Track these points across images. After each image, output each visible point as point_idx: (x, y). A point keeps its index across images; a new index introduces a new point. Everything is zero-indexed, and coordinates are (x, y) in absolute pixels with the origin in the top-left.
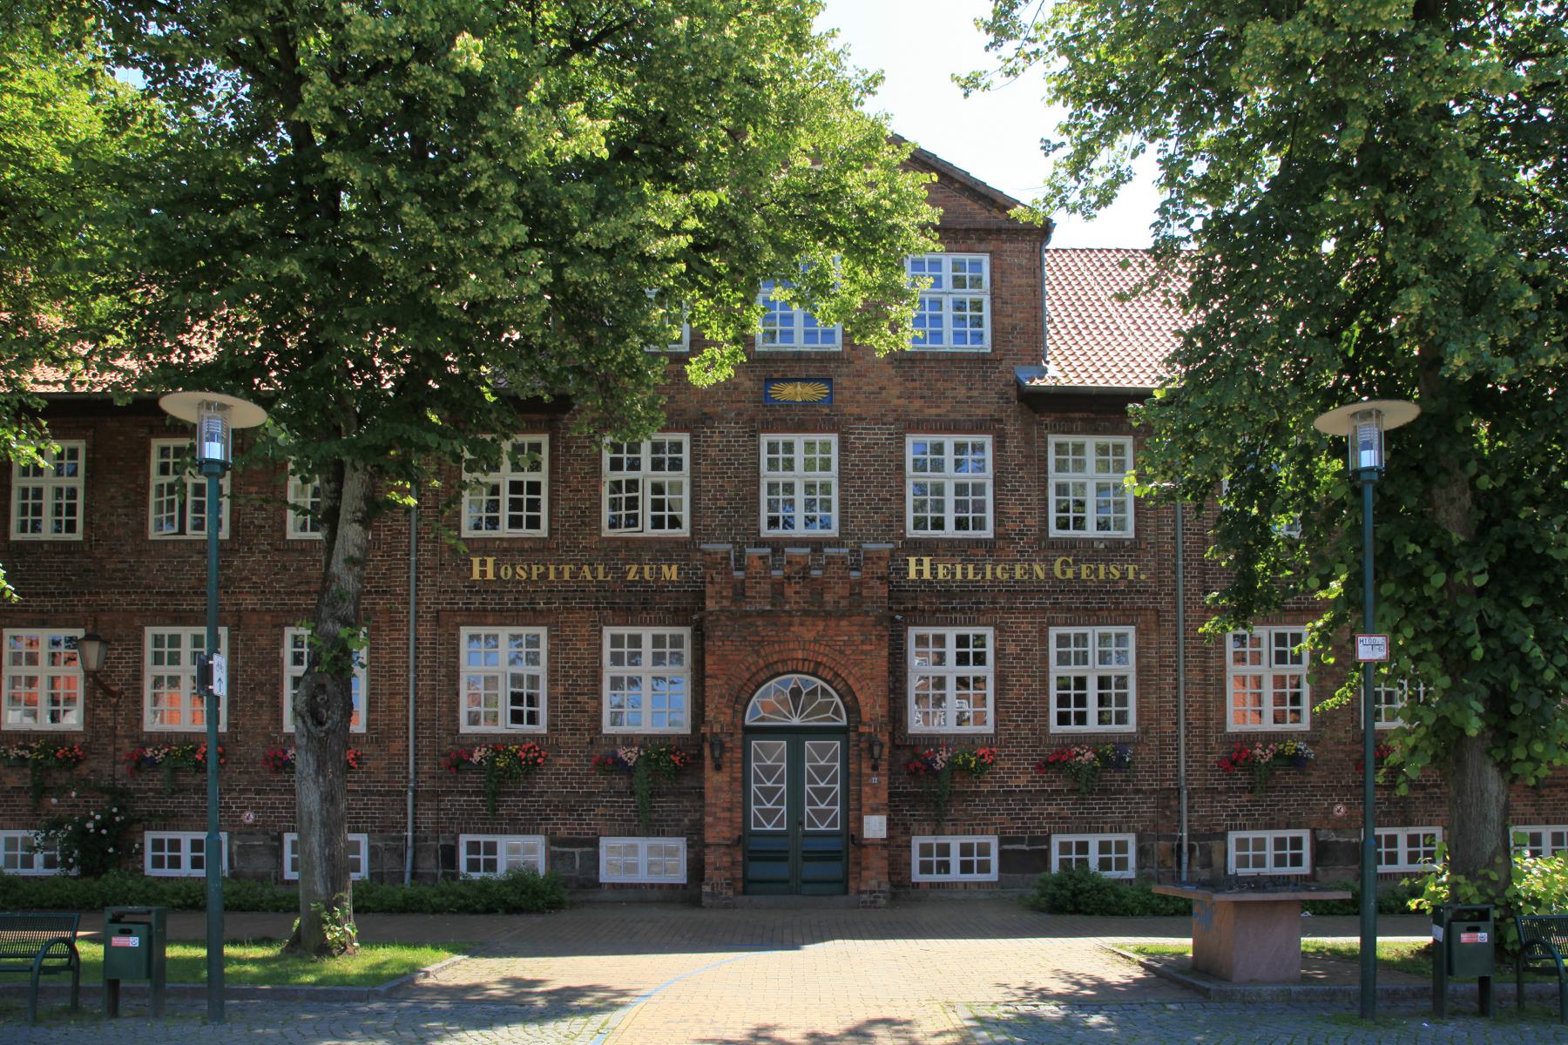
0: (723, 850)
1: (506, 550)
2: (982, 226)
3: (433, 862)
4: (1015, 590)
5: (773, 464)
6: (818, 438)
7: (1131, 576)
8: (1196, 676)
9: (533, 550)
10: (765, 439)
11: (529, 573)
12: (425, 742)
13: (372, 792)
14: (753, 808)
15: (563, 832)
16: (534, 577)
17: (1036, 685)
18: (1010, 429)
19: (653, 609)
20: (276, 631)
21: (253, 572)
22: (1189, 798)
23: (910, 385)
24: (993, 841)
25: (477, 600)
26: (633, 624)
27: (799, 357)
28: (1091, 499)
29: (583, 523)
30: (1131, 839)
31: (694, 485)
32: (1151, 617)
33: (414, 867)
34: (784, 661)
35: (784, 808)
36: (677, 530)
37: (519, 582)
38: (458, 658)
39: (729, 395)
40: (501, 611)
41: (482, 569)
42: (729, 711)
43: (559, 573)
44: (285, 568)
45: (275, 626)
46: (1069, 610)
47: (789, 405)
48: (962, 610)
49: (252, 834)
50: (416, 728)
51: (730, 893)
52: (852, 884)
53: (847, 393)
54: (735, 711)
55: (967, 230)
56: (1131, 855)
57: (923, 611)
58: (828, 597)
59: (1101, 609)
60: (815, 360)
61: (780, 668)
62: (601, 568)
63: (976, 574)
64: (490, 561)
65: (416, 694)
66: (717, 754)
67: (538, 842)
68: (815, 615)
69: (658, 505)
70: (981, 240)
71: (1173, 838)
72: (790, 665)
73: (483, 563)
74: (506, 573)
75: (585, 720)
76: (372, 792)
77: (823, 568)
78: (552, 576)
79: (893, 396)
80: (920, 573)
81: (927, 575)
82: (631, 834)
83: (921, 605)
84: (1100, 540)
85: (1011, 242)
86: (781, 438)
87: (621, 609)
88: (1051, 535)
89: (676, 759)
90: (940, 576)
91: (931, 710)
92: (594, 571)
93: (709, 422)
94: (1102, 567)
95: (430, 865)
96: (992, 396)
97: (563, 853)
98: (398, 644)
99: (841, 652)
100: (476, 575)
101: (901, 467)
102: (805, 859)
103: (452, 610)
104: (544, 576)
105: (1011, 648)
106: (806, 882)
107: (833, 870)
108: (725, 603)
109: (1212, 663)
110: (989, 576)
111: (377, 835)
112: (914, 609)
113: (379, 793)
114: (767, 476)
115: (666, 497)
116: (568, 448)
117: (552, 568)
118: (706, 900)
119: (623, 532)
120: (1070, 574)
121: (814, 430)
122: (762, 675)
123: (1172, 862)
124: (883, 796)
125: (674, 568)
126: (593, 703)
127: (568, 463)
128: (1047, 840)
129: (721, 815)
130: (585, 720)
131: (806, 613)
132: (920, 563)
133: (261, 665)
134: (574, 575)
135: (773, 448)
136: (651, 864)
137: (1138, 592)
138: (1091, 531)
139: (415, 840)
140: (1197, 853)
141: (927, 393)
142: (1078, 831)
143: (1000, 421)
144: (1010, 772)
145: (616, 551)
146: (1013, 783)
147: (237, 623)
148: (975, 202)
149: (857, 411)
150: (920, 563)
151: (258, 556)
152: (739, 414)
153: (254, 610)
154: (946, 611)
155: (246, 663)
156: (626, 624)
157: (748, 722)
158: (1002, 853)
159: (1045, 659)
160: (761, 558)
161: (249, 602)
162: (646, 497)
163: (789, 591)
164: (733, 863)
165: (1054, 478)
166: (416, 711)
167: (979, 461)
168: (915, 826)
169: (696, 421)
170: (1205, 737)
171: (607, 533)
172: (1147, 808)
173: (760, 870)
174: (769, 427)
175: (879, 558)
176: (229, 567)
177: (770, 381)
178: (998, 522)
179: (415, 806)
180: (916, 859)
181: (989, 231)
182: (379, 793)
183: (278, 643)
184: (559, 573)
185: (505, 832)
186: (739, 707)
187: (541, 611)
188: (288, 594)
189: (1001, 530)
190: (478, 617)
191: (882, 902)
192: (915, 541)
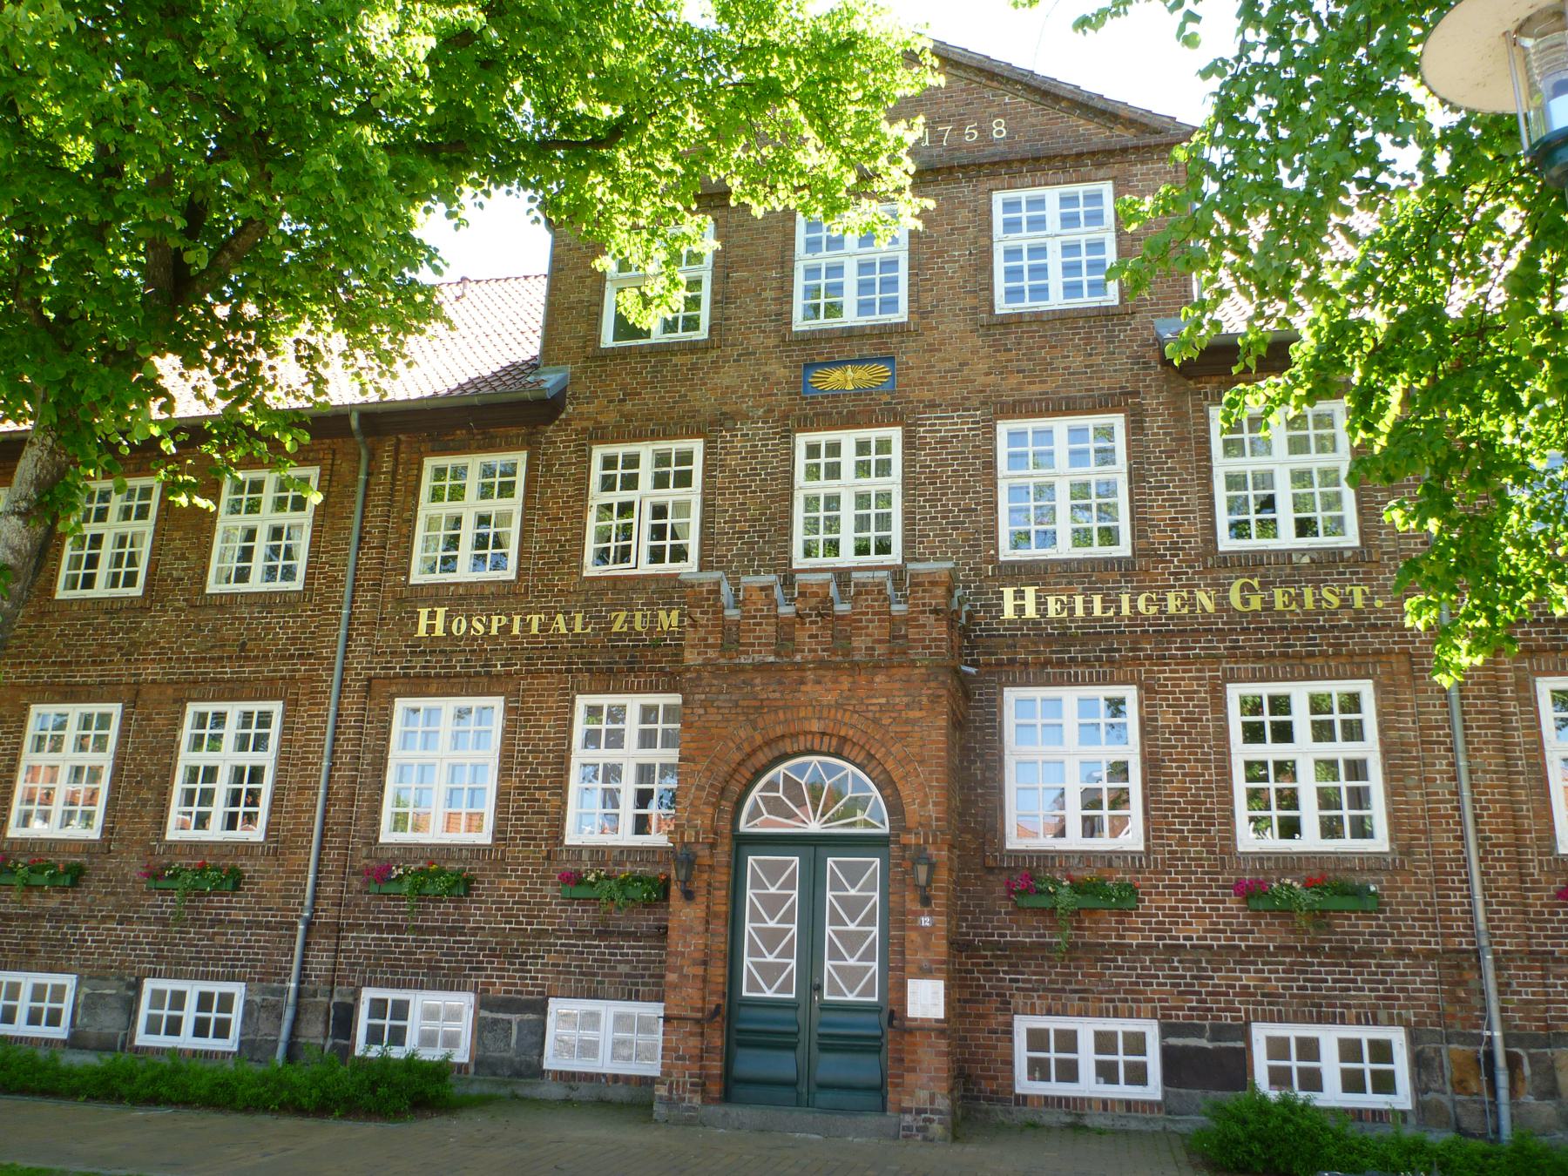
1: (462, 598)
2: (1100, 147)
3: (320, 1028)
4: (1166, 632)
5: (812, 473)
6: (872, 434)
7: (1359, 603)
8: (1489, 758)
9: (496, 596)
10: (802, 440)
11: (488, 627)
12: (333, 854)
13: (259, 925)
15: (498, 990)
16: (494, 632)
17: (1211, 774)
18: (1150, 402)
19: (642, 670)
20: (176, 707)
21: (162, 635)
22: (1499, 968)
23: (1002, 356)
24: (1151, 1030)
25: (418, 663)
26: (617, 691)
27: (850, 333)
28: (1284, 493)
29: (562, 559)
30: (1397, 1037)
31: (707, 505)
32: (1400, 665)
33: (293, 1033)
34: (794, 736)
35: (793, 962)
36: (682, 564)
37: (475, 638)
38: (387, 740)
39: (756, 388)
40: (447, 676)
41: (430, 622)
42: (709, 810)
43: (526, 625)
44: (199, 628)
45: (175, 701)
46: (1258, 657)
47: (836, 396)
48: (1085, 661)
49: (105, 979)
50: (323, 835)
51: (697, 1099)
52: (891, 1096)
53: (914, 374)
55: (1080, 155)
56: (1401, 1066)
57: (1026, 664)
58: (859, 642)
59: (1311, 655)
60: (871, 336)
61: (788, 746)
62: (579, 617)
63: (1105, 609)
64: (441, 612)
65: (328, 788)
67: (464, 1001)
68: (836, 667)
69: (658, 532)
70: (1099, 165)
71: (1478, 1039)
72: (802, 743)
73: (432, 616)
74: (459, 627)
75: (542, 825)
76: (259, 925)
77: (854, 600)
78: (516, 631)
79: (980, 372)
80: (1020, 609)
81: (1031, 612)
82: (593, 995)
84: (1303, 552)
85: (1143, 162)
86: (823, 437)
87: (600, 671)
88: (1221, 548)
90: (1051, 613)
92: (569, 622)
93: (729, 424)
94: (1308, 592)
95: (315, 1032)
96: (1122, 360)
97: (496, 1022)
98: (316, 722)
99: (875, 721)
100: (422, 631)
101: (991, 465)
102: (824, 1048)
103: (387, 677)
104: (505, 630)
105: (1166, 717)
106: (823, 1086)
107: (863, 1068)
108: (712, 654)
109: (1518, 737)
110: (1126, 610)
111: (256, 986)
112: (1012, 662)
113: (268, 926)
114: (803, 488)
115: (669, 521)
116: (549, 466)
117: (517, 619)
118: (659, 1110)
119: (614, 569)
120: (1256, 603)
121: (869, 425)
122: (762, 758)
123: (1478, 1084)
124: (941, 947)
125: (675, 614)
126: (556, 801)
127: (548, 485)
128: (1245, 1035)
129: (689, 970)
130: (542, 825)
131: (822, 664)
132: (1019, 595)
133: (153, 752)
134: (544, 628)
135: (813, 451)
136: (618, 1044)
137: (1374, 627)
138: (1287, 539)
139: (299, 993)
140: (1527, 1070)
141: (1025, 365)
142: (1298, 1018)
143: (1136, 393)
144: (1174, 914)
145: (601, 593)
146: (1179, 934)
147: (133, 697)
148: (1090, 120)
149: (927, 395)
150: (1019, 595)
151: (171, 615)
152: (770, 411)
153: (154, 682)
154: (1061, 663)
155: (136, 749)
156: (606, 691)
158: (1168, 1054)
159: (1223, 734)
160: (762, 589)
161: (151, 671)
162: (644, 522)
163: (802, 636)
165: (1222, 467)
166: (326, 812)
167: (1105, 450)
168: (1018, 1000)
169: (711, 424)
170: (1519, 864)
171: (591, 569)
172: (1422, 982)
173: (751, 1063)
174: (807, 425)
175: (933, 583)
176: (136, 629)
177: (810, 366)
178: (1138, 533)
179: (306, 945)
180: (1021, 1054)
181: (1110, 153)
182: (268, 926)
183: (176, 723)
184: (526, 625)
185: (420, 986)
186: (727, 806)
187: (498, 676)
188: (195, 660)
189: (1143, 543)
190: (420, 685)
191: (937, 1129)
192: (1012, 565)
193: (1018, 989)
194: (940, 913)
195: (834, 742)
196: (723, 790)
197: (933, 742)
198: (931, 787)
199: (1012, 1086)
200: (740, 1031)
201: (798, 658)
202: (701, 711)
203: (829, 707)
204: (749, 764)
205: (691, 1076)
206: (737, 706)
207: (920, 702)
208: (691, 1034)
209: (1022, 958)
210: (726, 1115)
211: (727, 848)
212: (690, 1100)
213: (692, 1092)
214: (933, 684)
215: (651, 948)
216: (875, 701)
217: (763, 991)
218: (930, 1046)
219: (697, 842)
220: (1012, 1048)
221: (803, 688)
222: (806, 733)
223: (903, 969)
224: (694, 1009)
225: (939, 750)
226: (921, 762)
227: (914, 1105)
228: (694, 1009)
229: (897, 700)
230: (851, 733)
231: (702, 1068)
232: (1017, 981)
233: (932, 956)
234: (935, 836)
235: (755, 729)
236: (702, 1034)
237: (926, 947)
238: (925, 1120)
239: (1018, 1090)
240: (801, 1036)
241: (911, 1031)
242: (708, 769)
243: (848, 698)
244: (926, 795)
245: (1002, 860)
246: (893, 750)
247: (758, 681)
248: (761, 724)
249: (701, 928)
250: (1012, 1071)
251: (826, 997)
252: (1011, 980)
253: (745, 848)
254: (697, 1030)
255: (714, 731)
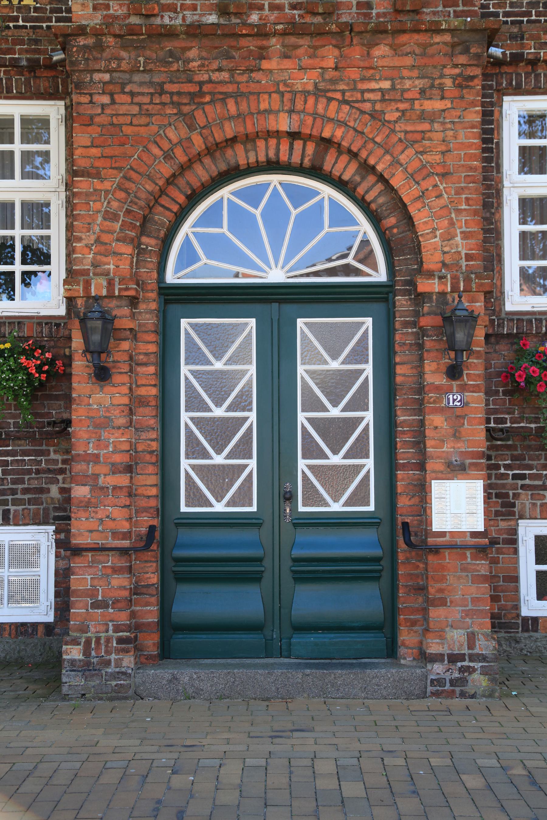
0: (111, 560)
14: (185, 464)
35: (252, 464)
42: (127, 249)
54: (140, 251)
66: (96, 338)
83: (530, 51)
89: (32, 365)
91: (103, 635)
99: (375, 115)
112: (517, 59)
157: (171, 278)
164: (136, 590)
193: (523, 487)
194: (475, 389)
195: (310, 148)
196: (145, 220)
197: (463, 146)
198: (459, 211)
199: (517, 607)
200: (179, 561)
201: (254, 18)
202: (106, 99)
203: (306, 93)
204: (181, 182)
205: (117, 629)
206: (162, 92)
207: (441, 88)
208: (115, 570)
209: (529, 448)
210: (175, 679)
211: (153, 306)
212: (118, 663)
213: (118, 651)
214: (462, 59)
215: (25, 453)
216: (374, 85)
217: (327, 505)
218: (464, 569)
219: (110, 296)
220: (516, 561)
221: (265, 65)
222: (269, 134)
223: (421, 466)
224: (115, 535)
225: (471, 157)
226: (444, 175)
227: (445, 650)
228: (115, 535)
229: (408, 84)
230: (339, 133)
231: (133, 615)
232: (523, 477)
233: (462, 447)
234: (468, 280)
235: (191, 128)
236: (130, 569)
237: (456, 435)
238: (462, 670)
239: (525, 612)
240: (267, 563)
241: (436, 550)
242: (120, 187)
243: (333, 81)
244: (452, 224)
245: (500, 325)
246: (403, 158)
247: (193, 53)
248: (201, 120)
249: (122, 421)
250: (517, 590)
251: (301, 509)
252: (515, 477)
253: (173, 308)
254: (122, 563)
255: (128, 130)
